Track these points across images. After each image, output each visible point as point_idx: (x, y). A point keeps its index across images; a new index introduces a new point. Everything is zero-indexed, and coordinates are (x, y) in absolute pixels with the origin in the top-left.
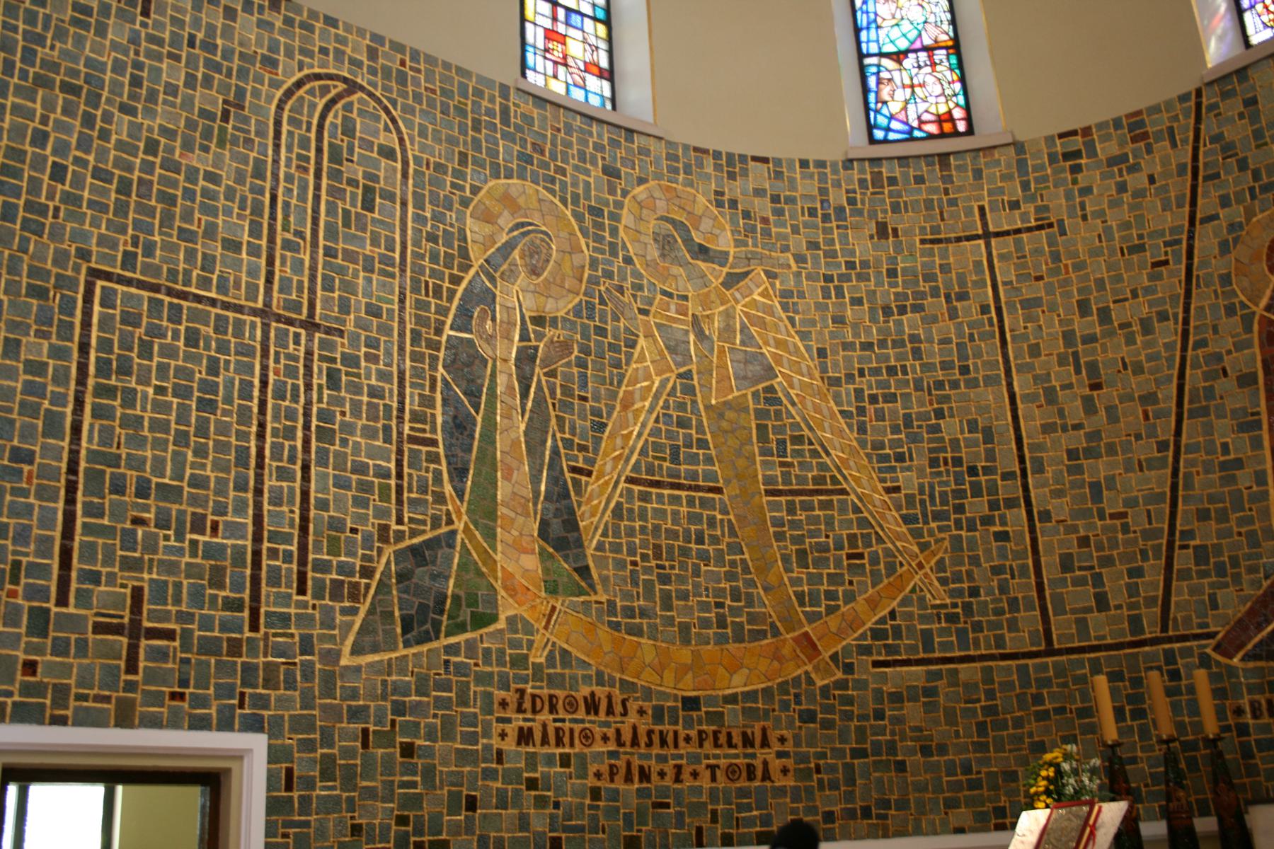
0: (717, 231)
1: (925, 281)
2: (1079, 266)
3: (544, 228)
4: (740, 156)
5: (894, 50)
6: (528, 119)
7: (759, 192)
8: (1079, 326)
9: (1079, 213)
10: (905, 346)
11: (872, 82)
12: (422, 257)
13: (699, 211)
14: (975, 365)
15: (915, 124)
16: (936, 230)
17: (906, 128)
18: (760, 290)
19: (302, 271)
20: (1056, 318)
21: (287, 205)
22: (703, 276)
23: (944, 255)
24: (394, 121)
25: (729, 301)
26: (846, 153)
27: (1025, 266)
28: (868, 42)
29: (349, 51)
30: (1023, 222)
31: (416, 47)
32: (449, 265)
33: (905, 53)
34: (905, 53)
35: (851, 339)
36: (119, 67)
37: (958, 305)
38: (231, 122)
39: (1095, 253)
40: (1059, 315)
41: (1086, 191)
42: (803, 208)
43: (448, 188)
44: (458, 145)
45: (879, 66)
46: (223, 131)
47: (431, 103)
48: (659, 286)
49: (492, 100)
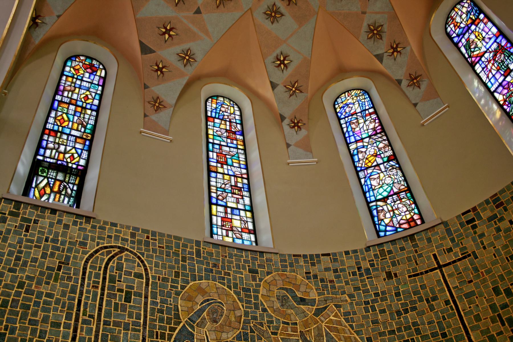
0: (308, 290)
1: (414, 295)
2: (489, 271)
3: (220, 301)
4: (316, 255)
5: (382, 197)
6: (211, 254)
7: (327, 269)
8: (497, 301)
9: (481, 246)
10: (410, 329)
11: (375, 212)
12: (155, 320)
13: (298, 283)
14: (449, 331)
15: (398, 226)
16: (415, 270)
17: (394, 228)
18: (333, 314)
19: (92, 333)
20: (484, 300)
21: (86, 304)
22: (304, 312)
23: (421, 281)
24: (142, 262)
25: (318, 322)
26: (366, 244)
27: (462, 277)
28: (370, 197)
29: (122, 235)
30: (456, 257)
31: (154, 230)
32: (169, 323)
33: (387, 198)
34: (387, 198)
35: (383, 330)
36: (11, 254)
37: (433, 303)
38: (62, 270)
39: (494, 263)
40: (485, 298)
41: (482, 235)
42: (349, 273)
43: (169, 288)
44: (174, 268)
45: (376, 205)
46: (57, 275)
47: (161, 253)
48: (282, 320)
49: (192, 248)
